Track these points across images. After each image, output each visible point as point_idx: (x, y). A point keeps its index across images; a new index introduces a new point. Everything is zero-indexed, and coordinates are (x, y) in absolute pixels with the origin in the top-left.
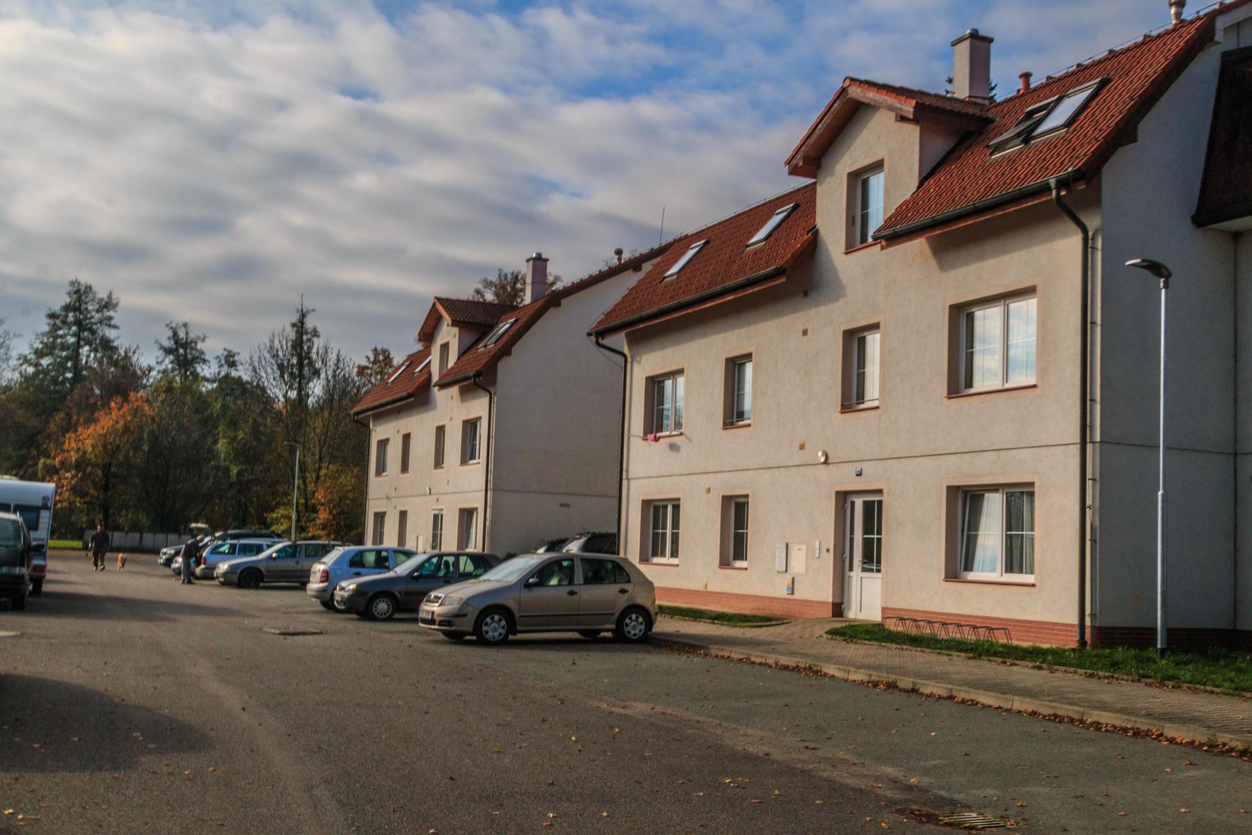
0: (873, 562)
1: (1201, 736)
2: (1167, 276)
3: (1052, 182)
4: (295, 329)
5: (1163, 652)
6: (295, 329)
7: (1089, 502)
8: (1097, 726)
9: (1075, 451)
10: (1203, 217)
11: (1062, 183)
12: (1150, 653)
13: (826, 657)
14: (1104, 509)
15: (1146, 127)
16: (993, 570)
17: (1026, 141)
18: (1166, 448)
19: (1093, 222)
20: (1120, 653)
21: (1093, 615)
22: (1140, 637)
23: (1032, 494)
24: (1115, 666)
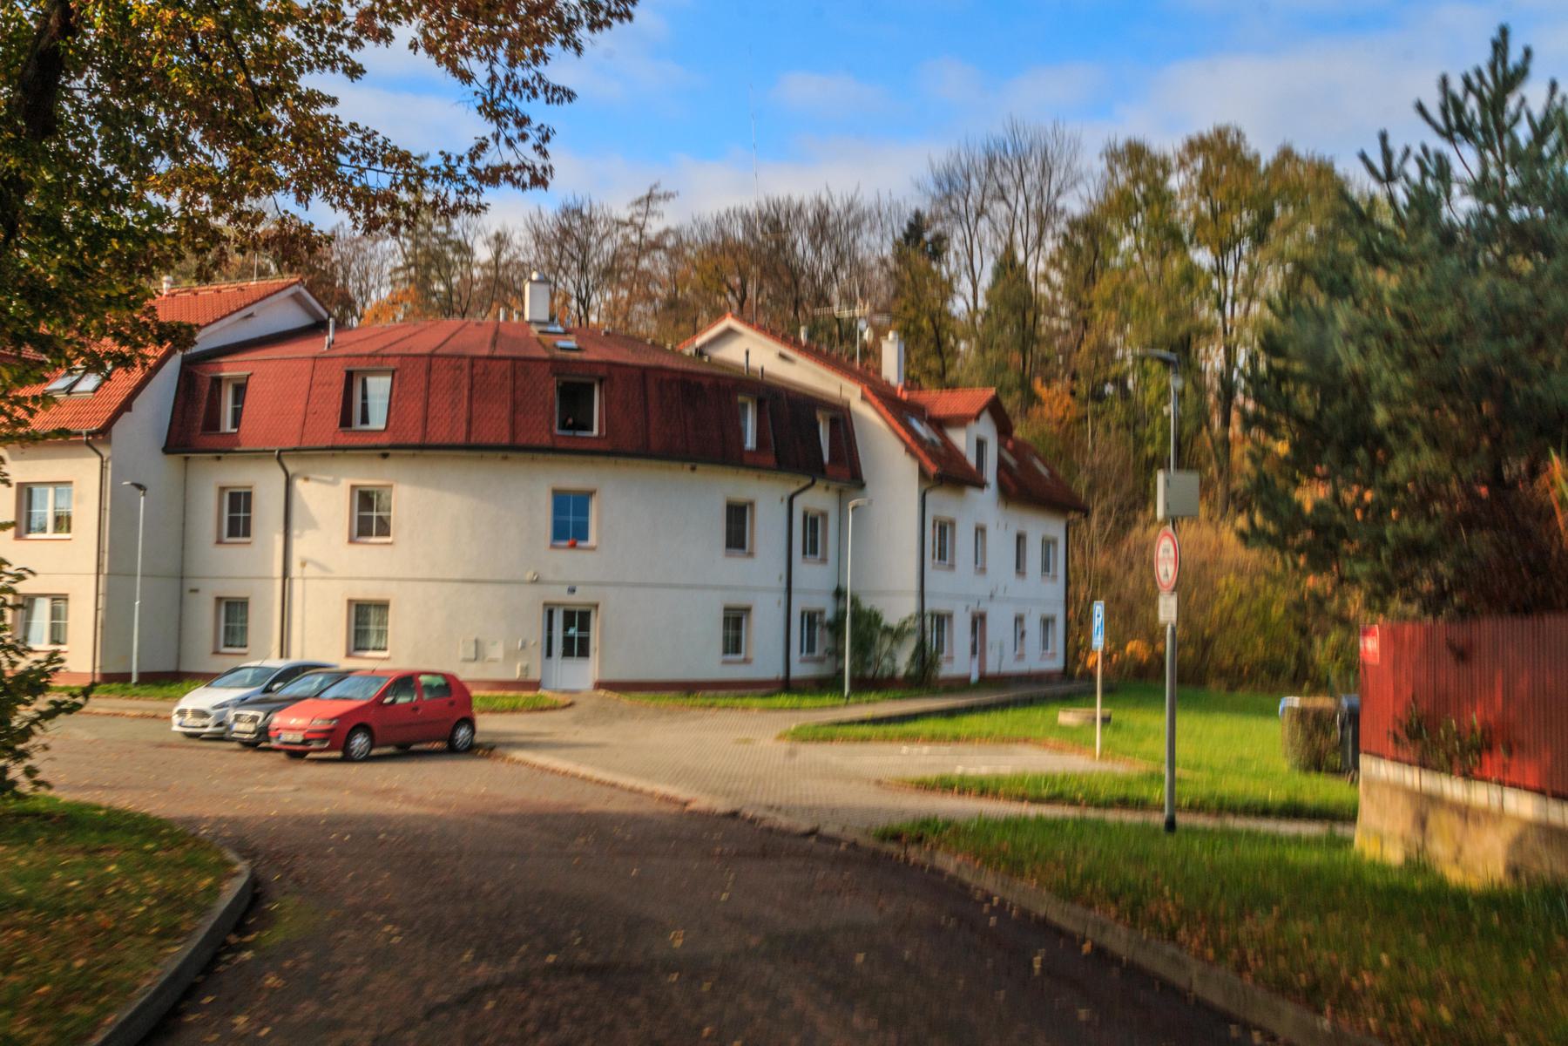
0: (1094, 693)
1: (139, 713)
2: (145, 490)
3: (84, 432)
4: (978, 896)
5: (136, 684)
6: (978, 896)
7: (100, 606)
8: (97, 714)
9: (93, 578)
10: (170, 448)
11: (88, 434)
12: (129, 685)
13: (1264, 235)
14: (108, 610)
15: (136, 403)
16: (41, 642)
17: (69, 393)
18: (142, 576)
19: (106, 452)
20: (114, 686)
21: (101, 667)
22: (124, 678)
23: (66, 600)
24: (110, 691)
